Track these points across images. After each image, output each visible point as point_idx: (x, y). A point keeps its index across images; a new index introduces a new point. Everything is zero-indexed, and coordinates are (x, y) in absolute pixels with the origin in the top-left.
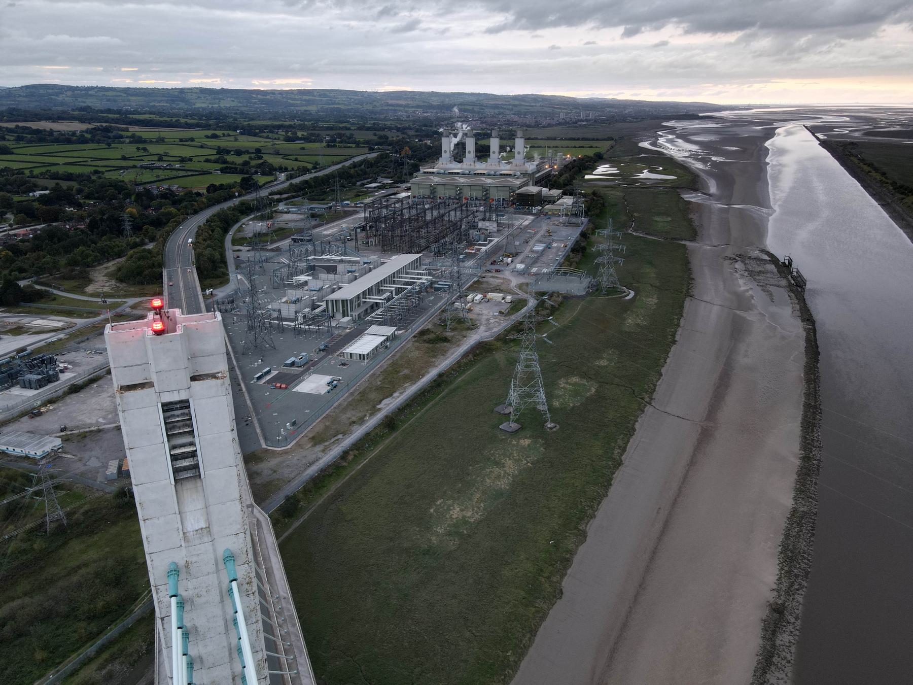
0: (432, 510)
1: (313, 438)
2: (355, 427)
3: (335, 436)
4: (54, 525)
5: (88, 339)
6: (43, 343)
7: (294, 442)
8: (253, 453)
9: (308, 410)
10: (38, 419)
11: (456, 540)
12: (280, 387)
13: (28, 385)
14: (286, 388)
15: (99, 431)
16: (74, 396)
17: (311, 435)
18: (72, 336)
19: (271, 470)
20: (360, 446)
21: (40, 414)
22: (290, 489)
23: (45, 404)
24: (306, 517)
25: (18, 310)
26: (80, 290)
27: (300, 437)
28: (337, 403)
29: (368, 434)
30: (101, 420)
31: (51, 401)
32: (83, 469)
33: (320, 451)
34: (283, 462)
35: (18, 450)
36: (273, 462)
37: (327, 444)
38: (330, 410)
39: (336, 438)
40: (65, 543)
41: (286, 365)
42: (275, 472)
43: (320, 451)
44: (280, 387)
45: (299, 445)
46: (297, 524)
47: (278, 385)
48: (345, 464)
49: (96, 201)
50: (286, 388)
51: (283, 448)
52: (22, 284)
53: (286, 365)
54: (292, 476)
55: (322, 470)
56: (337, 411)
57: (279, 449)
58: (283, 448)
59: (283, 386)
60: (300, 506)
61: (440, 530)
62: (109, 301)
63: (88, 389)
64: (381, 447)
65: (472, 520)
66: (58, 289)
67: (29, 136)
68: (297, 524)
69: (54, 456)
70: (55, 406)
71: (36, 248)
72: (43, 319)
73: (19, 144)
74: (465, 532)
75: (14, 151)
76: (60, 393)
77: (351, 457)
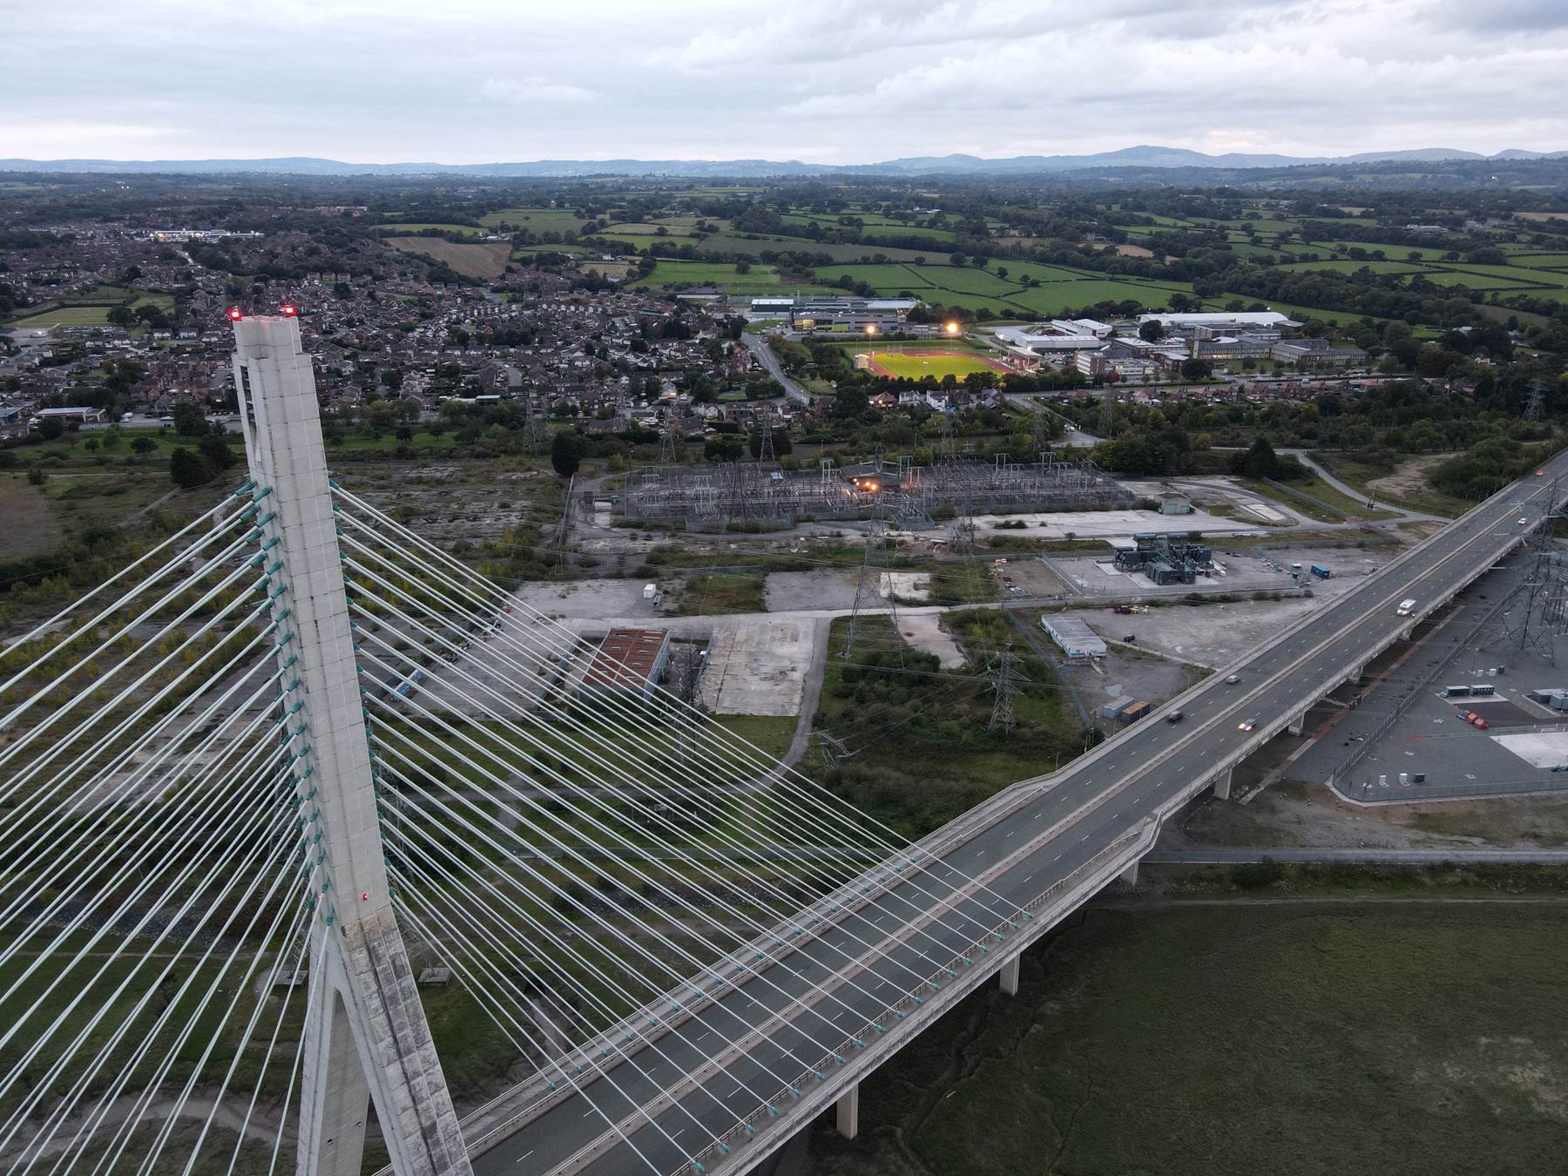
0: (1484, 1040)
1: (1423, 817)
2: (1531, 844)
3: (1469, 835)
4: (997, 726)
5: (1287, 548)
6: (1229, 534)
7: (1384, 804)
8: (1303, 782)
9: (1244, 730)
10: (1121, 616)
11: (1459, 1107)
12: (1473, 723)
13: (1152, 576)
14: (1483, 727)
15: (1161, 660)
16: (1185, 610)
17: (1423, 810)
18: (1275, 537)
19: (1298, 817)
20: (1487, 875)
21: (1127, 612)
22: (1283, 854)
23: (1142, 604)
24: (1267, 903)
25: (1251, 485)
26: (1357, 481)
27: (1404, 802)
28: (1545, 793)
29: (1534, 866)
30: (1179, 649)
31: (1154, 604)
32: (1096, 690)
33: (1409, 840)
34: (1330, 818)
35: (1060, 638)
36: (1313, 809)
37: (1435, 836)
38: (1515, 795)
39: (1465, 838)
40: (992, 751)
41: (1534, 697)
42: (1299, 823)
43: (1409, 840)
44: (1473, 723)
45: (1384, 813)
46: (1242, 902)
47: (1472, 717)
48: (1427, 880)
49: (1543, 353)
50: (1483, 727)
51: (1352, 801)
52: (1279, 452)
53: (1534, 697)
54: (1316, 842)
55: (1371, 863)
56: (1528, 803)
57: (1347, 800)
58: (1352, 801)
59: (1480, 722)
60: (1276, 885)
61: (1452, 1073)
62: (1379, 505)
63: (1210, 610)
64: (1537, 900)
65: (1541, 1109)
66: (1329, 471)
67: (1556, 236)
68: (1242, 902)
69: (1085, 662)
70: (1153, 610)
71: (1364, 409)
72: (1267, 505)
73: (1531, 249)
74: (1498, 1111)
75: (1510, 260)
76: (1174, 599)
77: (1450, 879)
